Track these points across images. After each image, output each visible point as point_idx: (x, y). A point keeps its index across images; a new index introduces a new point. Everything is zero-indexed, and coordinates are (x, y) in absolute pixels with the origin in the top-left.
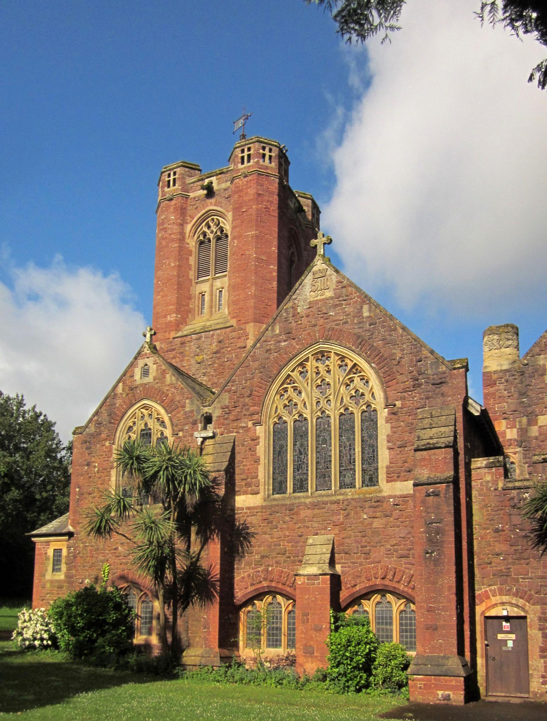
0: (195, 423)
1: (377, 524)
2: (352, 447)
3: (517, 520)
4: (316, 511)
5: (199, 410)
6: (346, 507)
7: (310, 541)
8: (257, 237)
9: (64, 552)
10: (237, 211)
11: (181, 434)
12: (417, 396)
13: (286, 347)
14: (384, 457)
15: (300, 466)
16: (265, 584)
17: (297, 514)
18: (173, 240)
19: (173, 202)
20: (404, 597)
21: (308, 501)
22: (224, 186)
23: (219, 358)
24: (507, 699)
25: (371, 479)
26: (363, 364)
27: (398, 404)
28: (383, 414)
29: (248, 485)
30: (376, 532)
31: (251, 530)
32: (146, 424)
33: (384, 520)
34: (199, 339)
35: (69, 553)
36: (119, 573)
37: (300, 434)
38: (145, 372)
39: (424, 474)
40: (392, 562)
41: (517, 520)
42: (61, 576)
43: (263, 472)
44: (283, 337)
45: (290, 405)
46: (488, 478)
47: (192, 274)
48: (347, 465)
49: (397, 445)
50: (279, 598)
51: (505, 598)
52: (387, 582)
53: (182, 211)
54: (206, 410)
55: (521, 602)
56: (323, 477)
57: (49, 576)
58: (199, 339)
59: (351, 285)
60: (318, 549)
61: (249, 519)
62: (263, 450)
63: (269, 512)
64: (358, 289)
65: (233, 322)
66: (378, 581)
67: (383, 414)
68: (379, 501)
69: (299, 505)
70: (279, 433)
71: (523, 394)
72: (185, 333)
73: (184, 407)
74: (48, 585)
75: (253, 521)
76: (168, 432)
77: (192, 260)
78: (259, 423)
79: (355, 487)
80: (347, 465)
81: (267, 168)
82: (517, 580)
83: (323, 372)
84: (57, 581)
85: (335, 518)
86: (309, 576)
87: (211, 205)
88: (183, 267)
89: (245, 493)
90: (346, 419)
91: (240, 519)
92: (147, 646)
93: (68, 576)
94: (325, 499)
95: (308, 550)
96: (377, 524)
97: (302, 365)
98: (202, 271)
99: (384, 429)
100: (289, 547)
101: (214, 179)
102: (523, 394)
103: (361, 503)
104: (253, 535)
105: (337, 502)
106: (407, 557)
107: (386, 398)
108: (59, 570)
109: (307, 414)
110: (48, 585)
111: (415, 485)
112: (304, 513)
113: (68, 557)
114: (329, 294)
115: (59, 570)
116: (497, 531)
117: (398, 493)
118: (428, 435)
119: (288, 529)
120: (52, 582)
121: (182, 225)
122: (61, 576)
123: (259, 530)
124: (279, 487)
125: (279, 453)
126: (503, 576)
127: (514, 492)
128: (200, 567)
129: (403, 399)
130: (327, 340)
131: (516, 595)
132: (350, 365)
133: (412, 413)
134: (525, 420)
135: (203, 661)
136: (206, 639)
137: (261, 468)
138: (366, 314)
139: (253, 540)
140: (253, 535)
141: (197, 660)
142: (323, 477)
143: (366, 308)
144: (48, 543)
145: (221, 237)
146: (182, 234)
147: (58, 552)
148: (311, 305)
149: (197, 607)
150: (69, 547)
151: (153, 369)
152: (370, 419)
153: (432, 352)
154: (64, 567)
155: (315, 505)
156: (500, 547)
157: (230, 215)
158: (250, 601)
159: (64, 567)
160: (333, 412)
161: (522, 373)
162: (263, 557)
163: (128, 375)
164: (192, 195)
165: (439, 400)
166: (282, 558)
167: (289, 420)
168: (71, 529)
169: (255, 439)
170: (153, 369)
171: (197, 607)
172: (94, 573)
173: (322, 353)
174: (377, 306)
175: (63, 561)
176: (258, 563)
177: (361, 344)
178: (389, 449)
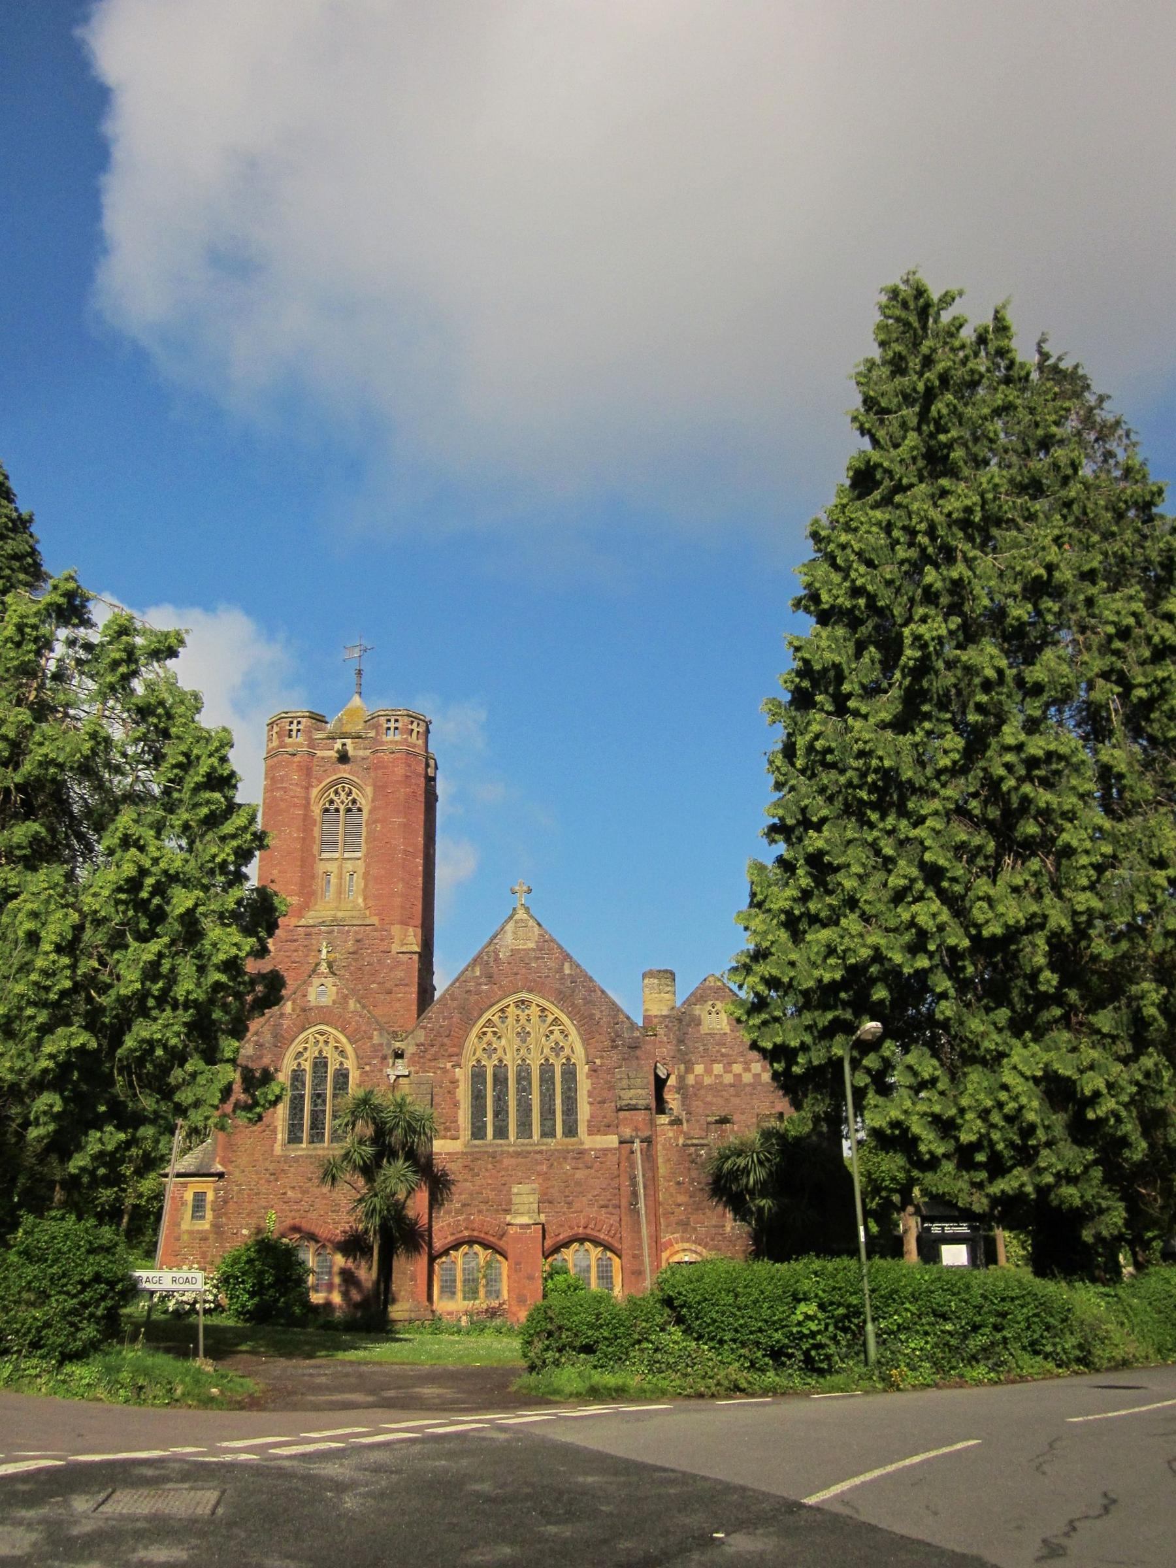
0: (384, 1058)
1: (579, 1175)
2: (552, 1098)
3: (694, 1174)
4: (520, 1160)
5: (389, 1045)
6: (550, 1157)
7: (515, 1190)
8: (405, 825)
9: (210, 1196)
10: (379, 788)
11: (367, 1068)
12: (615, 1056)
13: (487, 991)
14: (584, 1110)
15: (500, 1112)
16: (466, 1233)
17: (501, 1162)
18: (295, 805)
19: (296, 759)
20: (601, 1245)
21: (511, 1149)
22: (361, 753)
23: (356, 960)
25: (571, 1130)
26: (564, 1018)
27: (598, 1061)
28: (582, 1071)
29: (447, 1129)
30: (578, 1183)
31: (451, 1177)
32: (320, 1052)
33: (587, 1172)
34: (331, 932)
35: (217, 1197)
36: (289, 1222)
37: (500, 1080)
38: (322, 994)
39: (627, 1132)
40: (593, 1212)
41: (694, 1174)
42: (205, 1225)
43: (464, 1117)
44: (483, 980)
45: (489, 1051)
46: (671, 1134)
48: (548, 1113)
49: (598, 1102)
50: (477, 1247)
51: (686, 1245)
52: (589, 1231)
53: (307, 772)
54: (398, 1045)
55: (699, 1249)
56: (525, 1127)
57: (186, 1224)
58: (331, 932)
59: (553, 940)
60: (525, 1199)
61: (448, 1166)
62: (463, 1093)
63: (471, 1159)
64: (560, 947)
65: (375, 920)
66: (581, 1230)
68: (582, 1153)
69: (503, 1153)
70: (478, 1076)
71: (681, 1041)
72: (311, 922)
73: (371, 1038)
74: (185, 1237)
75: (454, 1169)
76: (350, 1064)
78: (459, 1066)
79: (554, 1136)
80: (548, 1113)
81: (414, 746)
82: (695, 1229)
83: (523, 1021)
84: (199, 1232)
85: (539, 1168)
86: (522, 1226)
87: (344, 771)
89: (445, 1138)
91: (439, 1163)
92: (328, 1305)
93: (216, 1226)
94: (529, 1148)
95: (516, 1200)
96: (579, 1175)
97: (502, 1011)
99: (584, 1084)
100: (492, 1195)
101: (348, 741)
102: (681, 1041)
103: (564, 1154)
104: (453, 1182)
105: (541, 1152)
106: (606, 1207)
107: (587, 1056)
108: (203, 1218)
110: (185, 1237)
111: (621, 1142)
112: (506, 1162)
113: (867, 1243)
114: (531, 945)
115: (203, 1218)
116: (678, 1183)
117: (598, 1146)
118: (628, 1096)
119: (491, 1177)
120: (191, 1232)
121: (307, 788)
122: (205, 1225)
123: (460, 1178)
124: (478, 1132)
125: (478, 1097)
126: (684, 1225)
127: (692, 1149)
128: (406, 1217)
129: (602, 1057)
130: (530, 991)
131: (695, 1242)
132: (550, 1018)
133: (610, 1071)
134: (682, 1067)
135: (413, 1315)
136: (412, 1293)
137: (461, 1113)
138: (567, 972)
139: (453, 1188)
140: (453, 1182)
141: (406, 1315)
142: (525, 1127)
143: (567, 965)
144: (185, 1185)
146: (308, 799)
147: (199, 1198)
148: (514, 952)
149: (403, 1259)
150: (217, 1190)
152: (570, 1074)
153: (628, 1018)
154: (209, 1215)
155: (518, 1154)
156: (681, 1199)
157: (369, 790)
158: (446, 1252)
159: (209, 1215)
161: (680, 1021)
162: (464, 1205)
163: (299, 994)
164: (319, 753)
165: (635, 1063)
166: (483, 1207)
167: (489, 1066)
168: (219, 1168)
171: (403, 1259)
172: (253, 1222)
173: (523, 1002)
174: (578, 966)
175: (208, 1207)
176: (459, 1212)
178: (591, 1104)
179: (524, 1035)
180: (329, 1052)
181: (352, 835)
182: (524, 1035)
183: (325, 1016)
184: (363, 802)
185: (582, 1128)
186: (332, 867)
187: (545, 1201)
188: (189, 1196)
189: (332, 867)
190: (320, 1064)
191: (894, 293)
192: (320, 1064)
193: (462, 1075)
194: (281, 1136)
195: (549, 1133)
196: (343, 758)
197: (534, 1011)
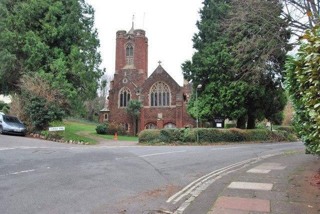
6: (164, 109)
10: (136, 44)
14: (170, 101)
15: (160, 100)
24: (213, 180)
38: (125, 81)
47: (126, 55)
48: (164, 101)
67: (170, 94)
70: (152, 94)
76: (130, 93)
77: (125, 52)
80: (164, 101)
88: (123, 54)
90: (164, 94)
93: (109, 120)
98: (128, 55)
109: (157, 93)
122: (107, 120)
124: (152, 105)
145: (132, 48)
147: (106, 115)
151: (127, 81)
152: (168, 93)
160: (162, 92)
167: (166, 92)
169: (148, 97)
170: (123, 81)
177: (167, 82)
179: (160, 88)
180: (127, 91)
181: (132, 53)
182: (160, 88)
183: (125, 85)
184: (133, 47)
185: (170, 104)
186: (128, 59)
187: (163, 117)
188: (104, 115)
189: (128, 59)
190: (125, 93)
191: (183, 65)
192: (125, 93)
193: (149, 95)
194: (119, 105)
195: (164, 105)
196: (129, 38)
197: (162, 84)
